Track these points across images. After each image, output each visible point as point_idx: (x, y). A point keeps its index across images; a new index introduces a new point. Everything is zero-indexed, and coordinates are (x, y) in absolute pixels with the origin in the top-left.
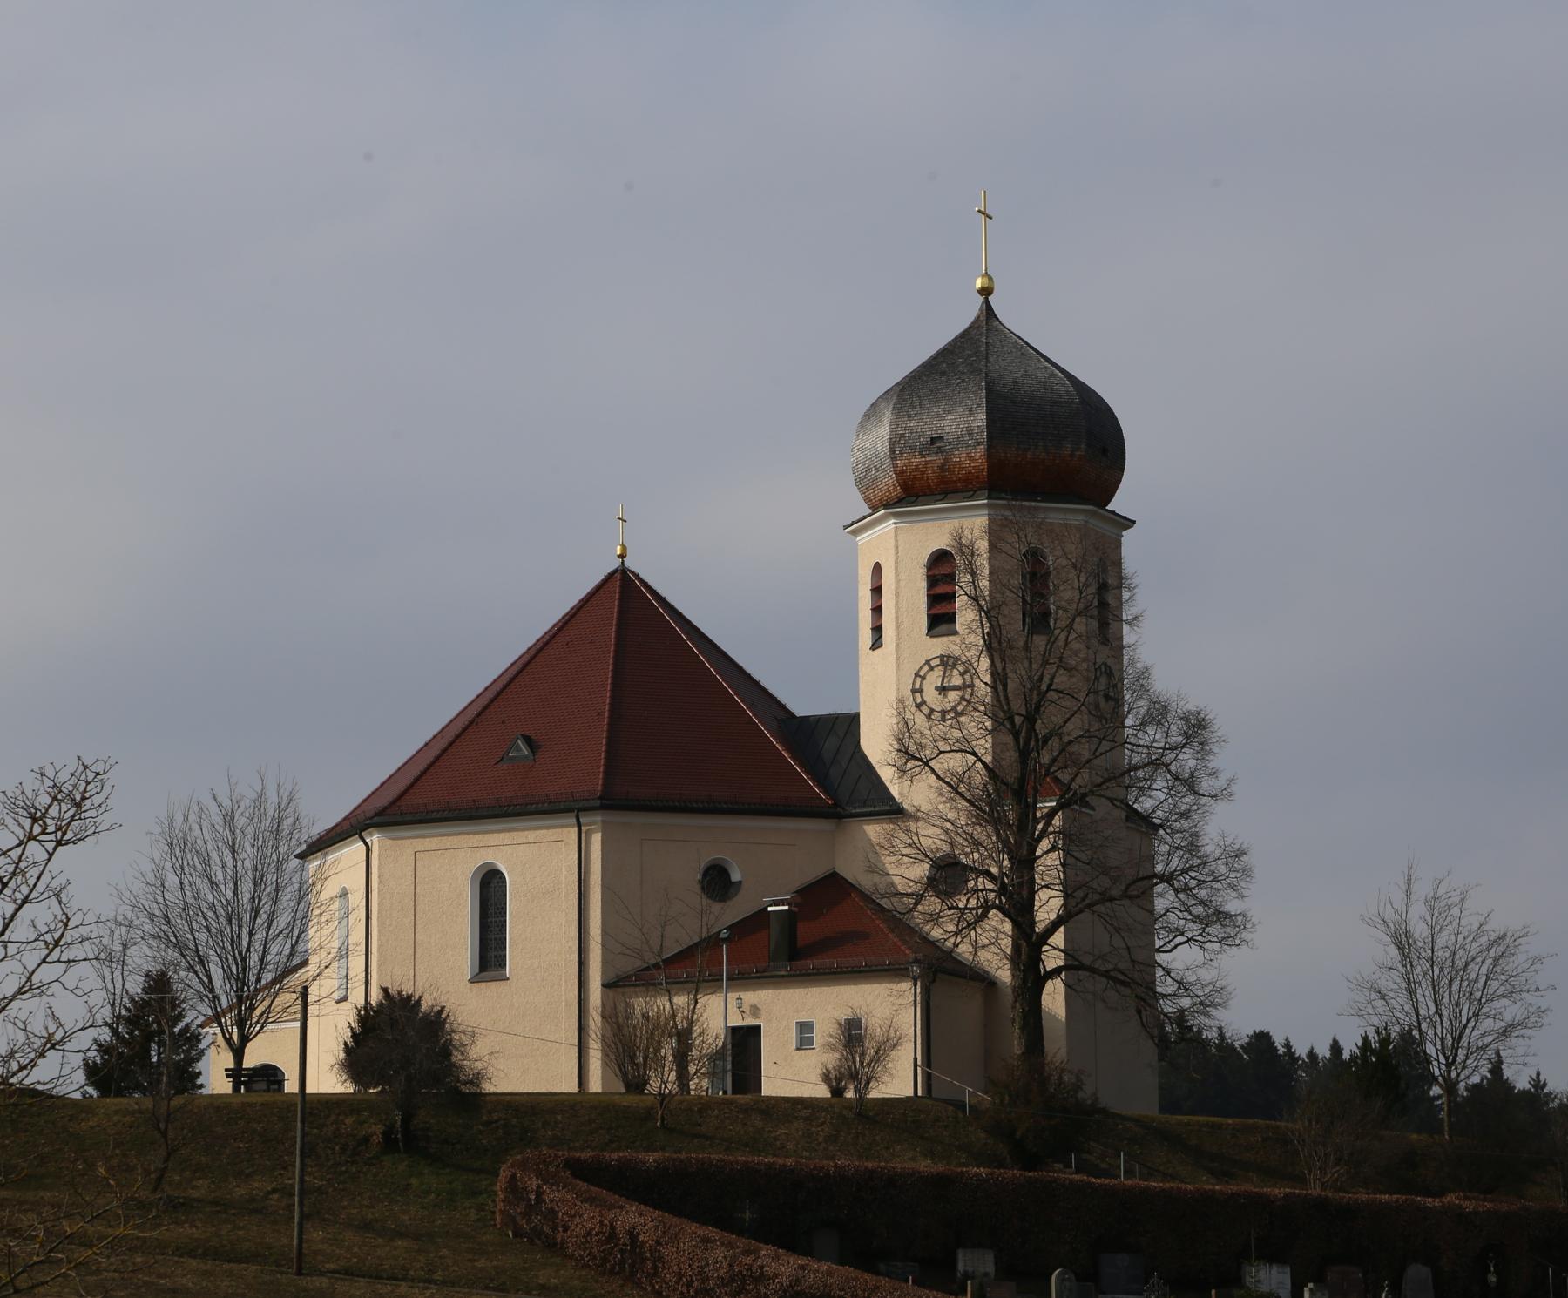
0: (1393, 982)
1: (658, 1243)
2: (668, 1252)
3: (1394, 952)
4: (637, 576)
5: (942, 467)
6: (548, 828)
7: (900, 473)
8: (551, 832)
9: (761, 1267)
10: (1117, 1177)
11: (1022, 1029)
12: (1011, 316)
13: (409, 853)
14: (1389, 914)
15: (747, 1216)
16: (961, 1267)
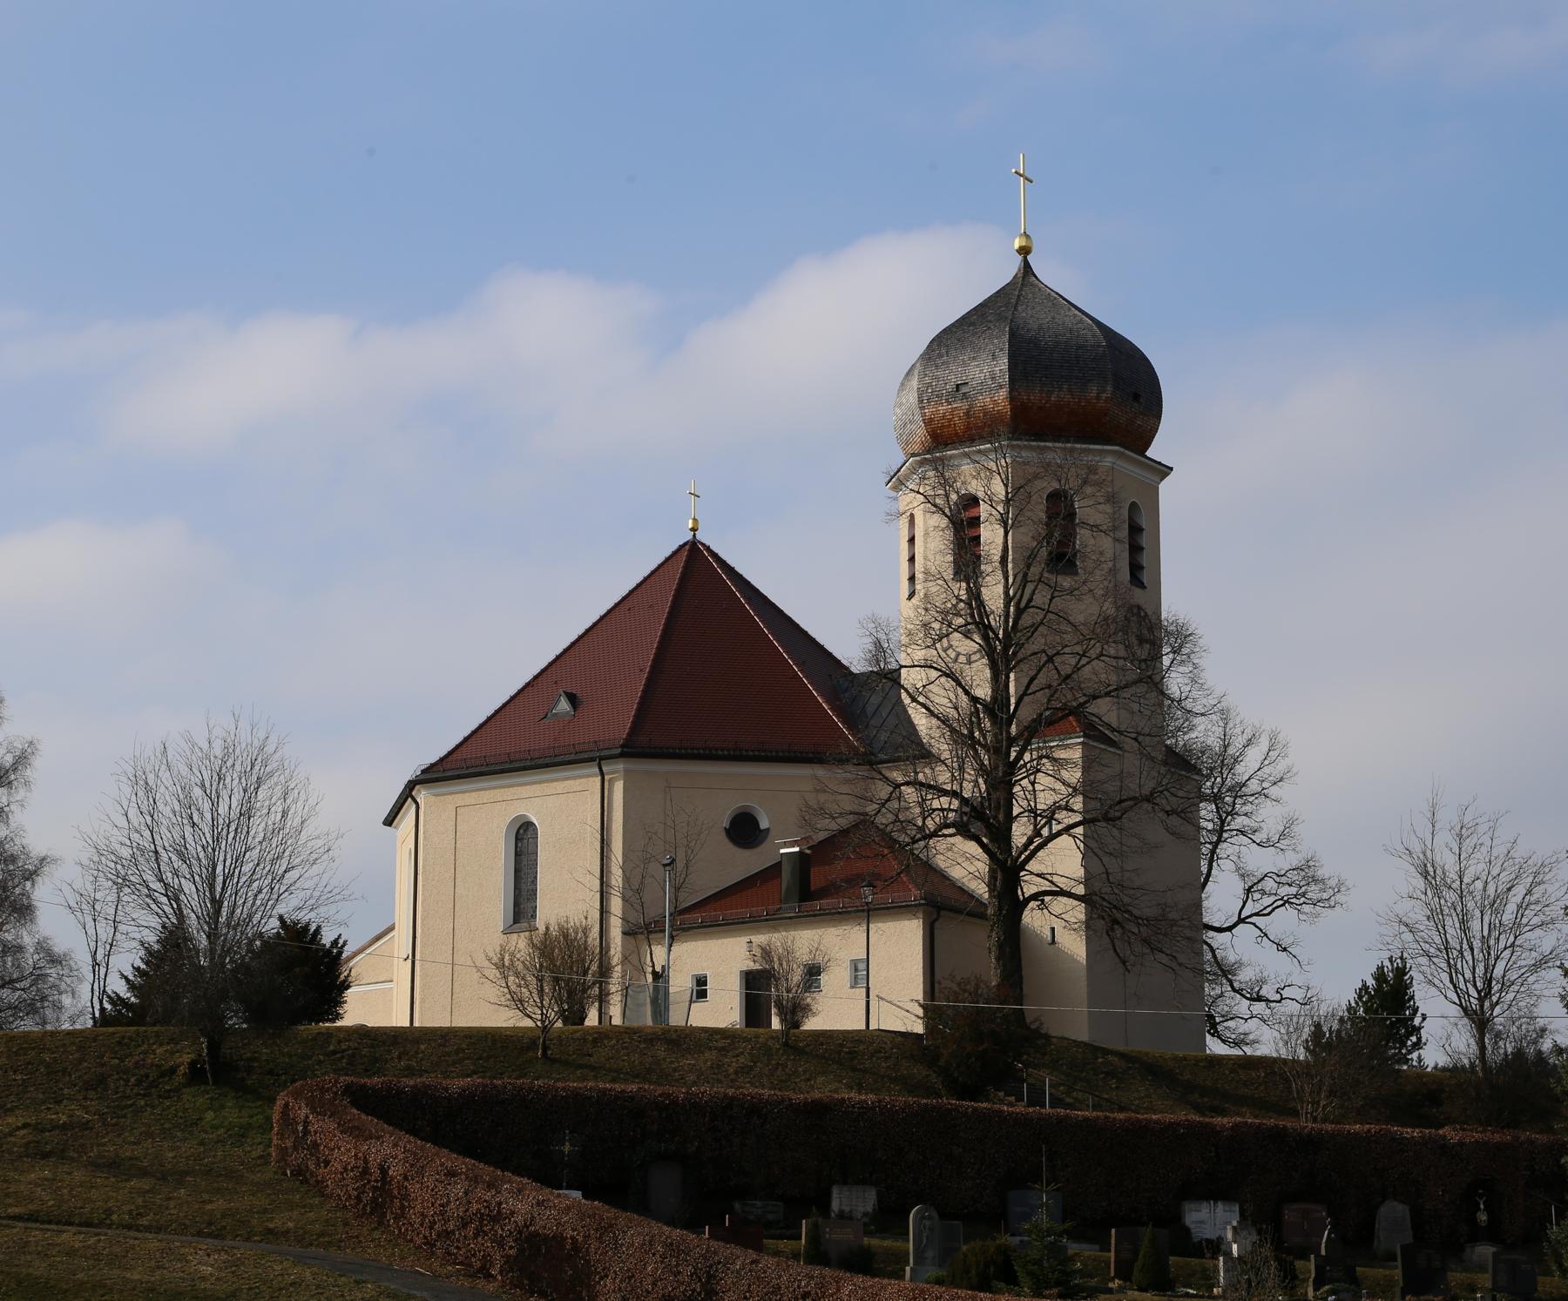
0: (1418, 914)
1: (406, 1178)
2: (413, 1188)
3: (1420, 883)
4: (708, 549)
5: (967, 413)
6: (574, 778)
7: (928, 422)
8: (578, 781)
9: (500, 1204)
10: (1044, 1106)
11: (998, 959)
12: (1050, 274)
13: (452, 808)
14: (1417, 848)
15: (567, 1148)
16: (835, 1205)
